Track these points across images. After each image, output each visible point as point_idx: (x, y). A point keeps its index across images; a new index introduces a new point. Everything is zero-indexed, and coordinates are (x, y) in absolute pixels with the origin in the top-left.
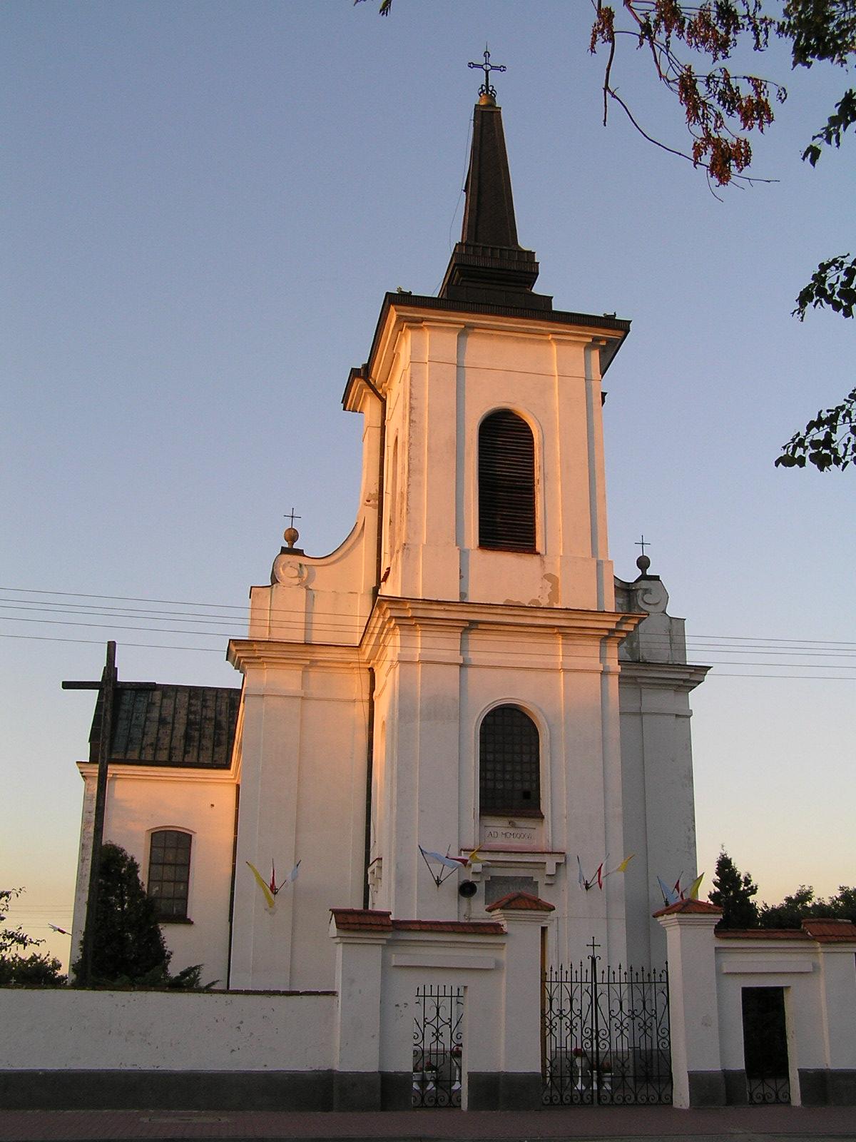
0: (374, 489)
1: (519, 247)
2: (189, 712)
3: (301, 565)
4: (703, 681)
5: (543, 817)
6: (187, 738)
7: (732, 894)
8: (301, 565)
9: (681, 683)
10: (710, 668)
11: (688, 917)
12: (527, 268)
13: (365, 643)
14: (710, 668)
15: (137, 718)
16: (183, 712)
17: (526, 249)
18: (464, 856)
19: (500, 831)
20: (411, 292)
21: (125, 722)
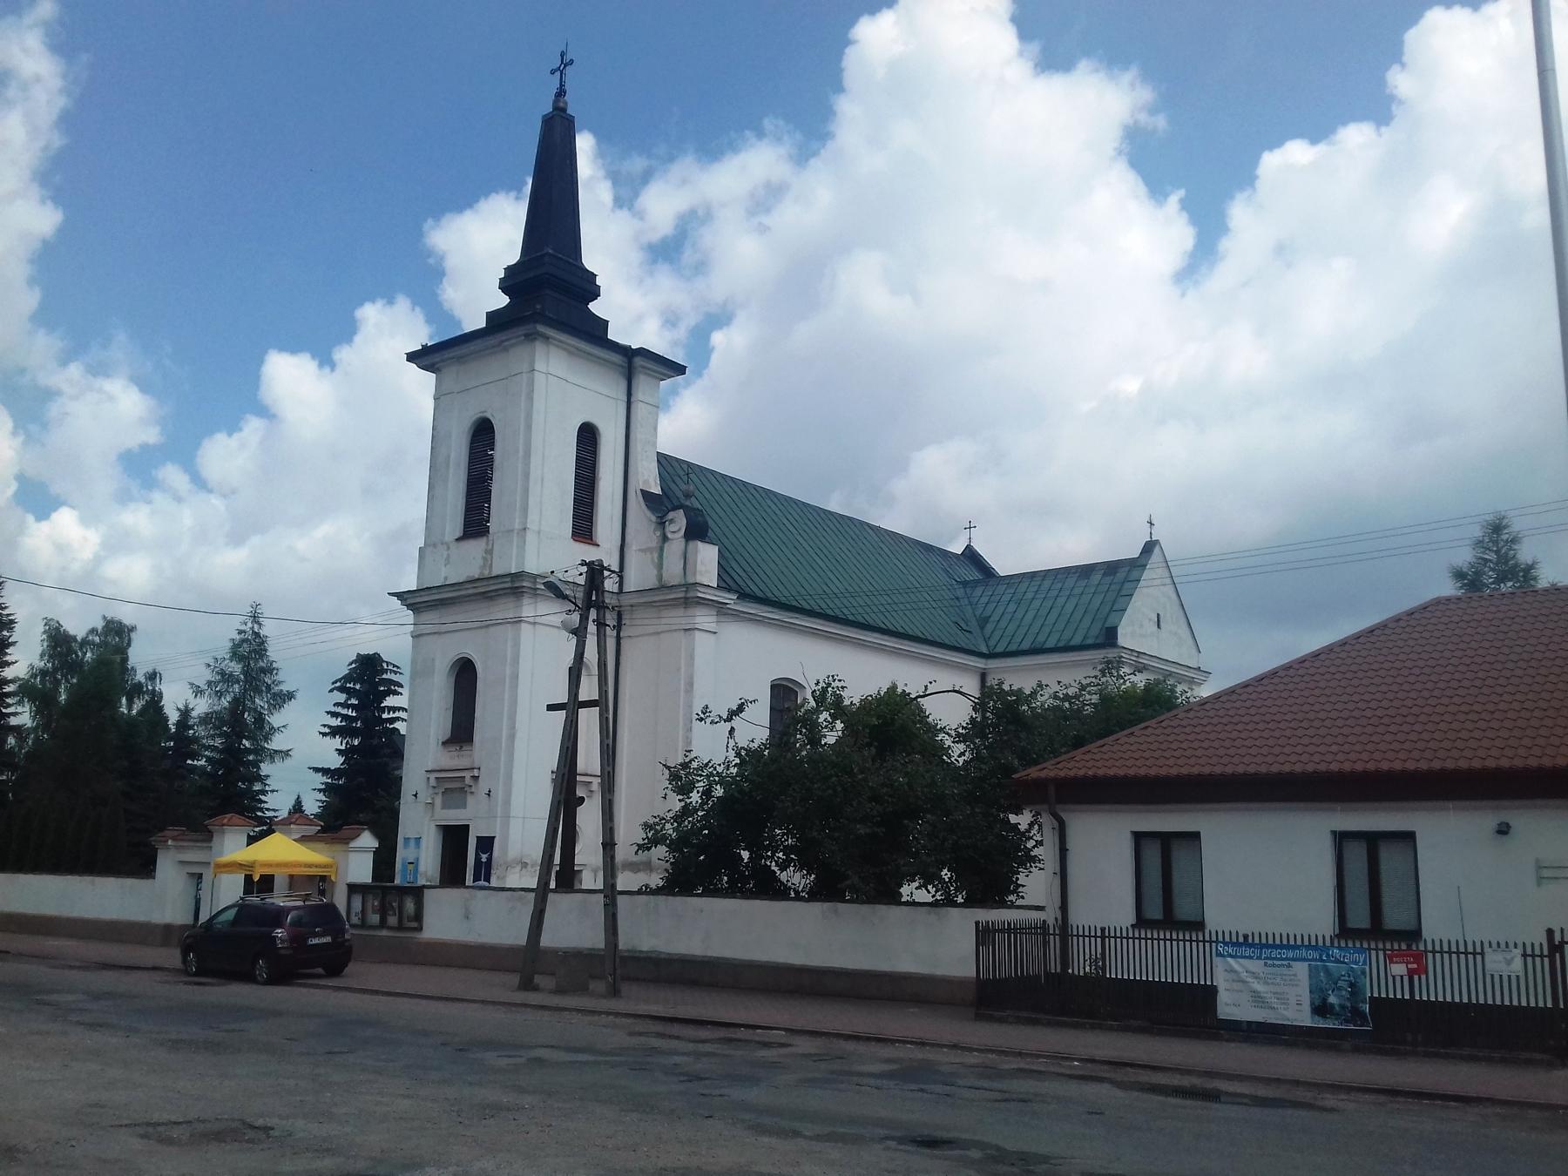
12: (588, 287)
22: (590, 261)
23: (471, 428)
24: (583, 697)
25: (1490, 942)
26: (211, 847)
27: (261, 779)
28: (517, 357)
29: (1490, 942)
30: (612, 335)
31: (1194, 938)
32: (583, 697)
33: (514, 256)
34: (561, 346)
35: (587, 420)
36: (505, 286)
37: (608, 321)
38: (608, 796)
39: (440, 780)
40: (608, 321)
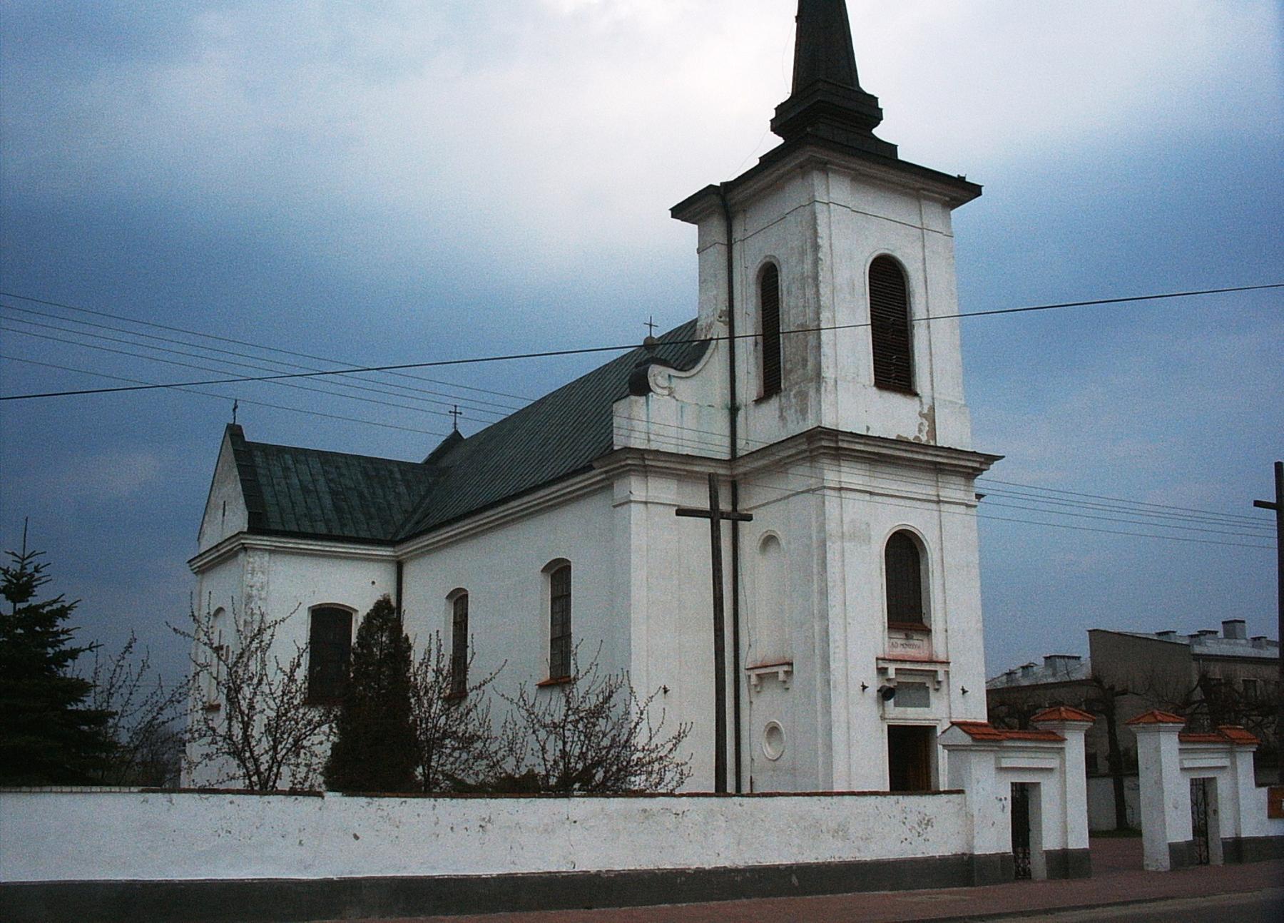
0: (724, 306)
1: (860, 88)
2: (329, 481)
3: (669, 376)
4: (988, 469)
5: (930, 631)
6: (337, 509)
7: (20, 631)
8: (669, 376)
9: (971, 471)
10: (991, 459)
11: (1016, 745)
12: (870, 111)
13: (774, 451)
14: (991, 459)
15: (279, 485)
16: (322, 480)
17: (868, 92)
18: (882, 664)
19: (899, 642)
20: (964, 178)
21: (270, 489)
22: (868, 82)
23: (758, 277)
24: (706, 505)
25: (1003, 810)
26: (1062, 749)
27: (79, 688)
28: (794, 195)
29: (1003, 810)
30: (902, 156)
31: (725, 506)
32: (706, 505)
33: (784, 91)
34: (844, 171)
35: (898, 255)
36: (777, 126)
37: (896, 146)
38: (719, 633)
39: (900, 672)
40: (896, 146)
